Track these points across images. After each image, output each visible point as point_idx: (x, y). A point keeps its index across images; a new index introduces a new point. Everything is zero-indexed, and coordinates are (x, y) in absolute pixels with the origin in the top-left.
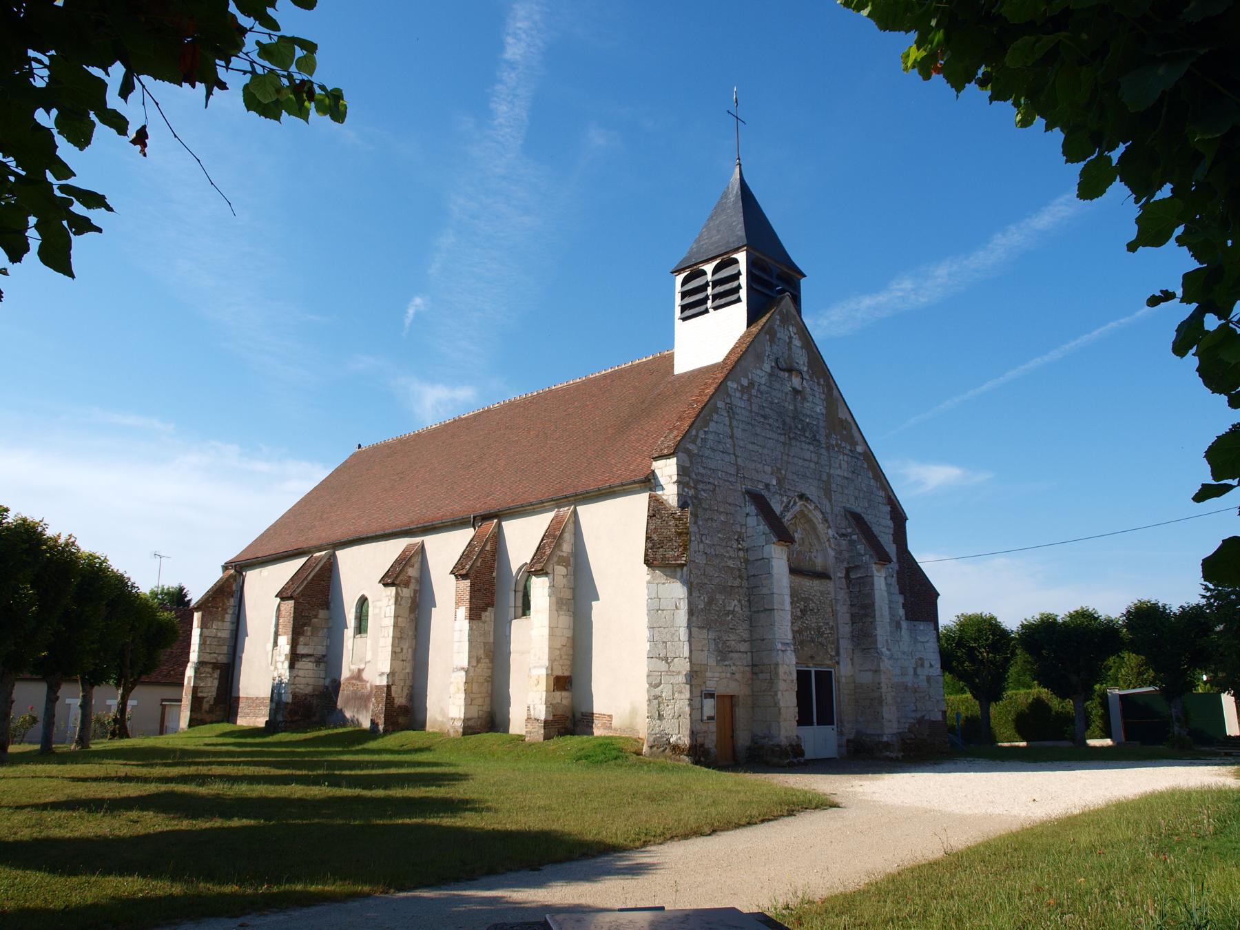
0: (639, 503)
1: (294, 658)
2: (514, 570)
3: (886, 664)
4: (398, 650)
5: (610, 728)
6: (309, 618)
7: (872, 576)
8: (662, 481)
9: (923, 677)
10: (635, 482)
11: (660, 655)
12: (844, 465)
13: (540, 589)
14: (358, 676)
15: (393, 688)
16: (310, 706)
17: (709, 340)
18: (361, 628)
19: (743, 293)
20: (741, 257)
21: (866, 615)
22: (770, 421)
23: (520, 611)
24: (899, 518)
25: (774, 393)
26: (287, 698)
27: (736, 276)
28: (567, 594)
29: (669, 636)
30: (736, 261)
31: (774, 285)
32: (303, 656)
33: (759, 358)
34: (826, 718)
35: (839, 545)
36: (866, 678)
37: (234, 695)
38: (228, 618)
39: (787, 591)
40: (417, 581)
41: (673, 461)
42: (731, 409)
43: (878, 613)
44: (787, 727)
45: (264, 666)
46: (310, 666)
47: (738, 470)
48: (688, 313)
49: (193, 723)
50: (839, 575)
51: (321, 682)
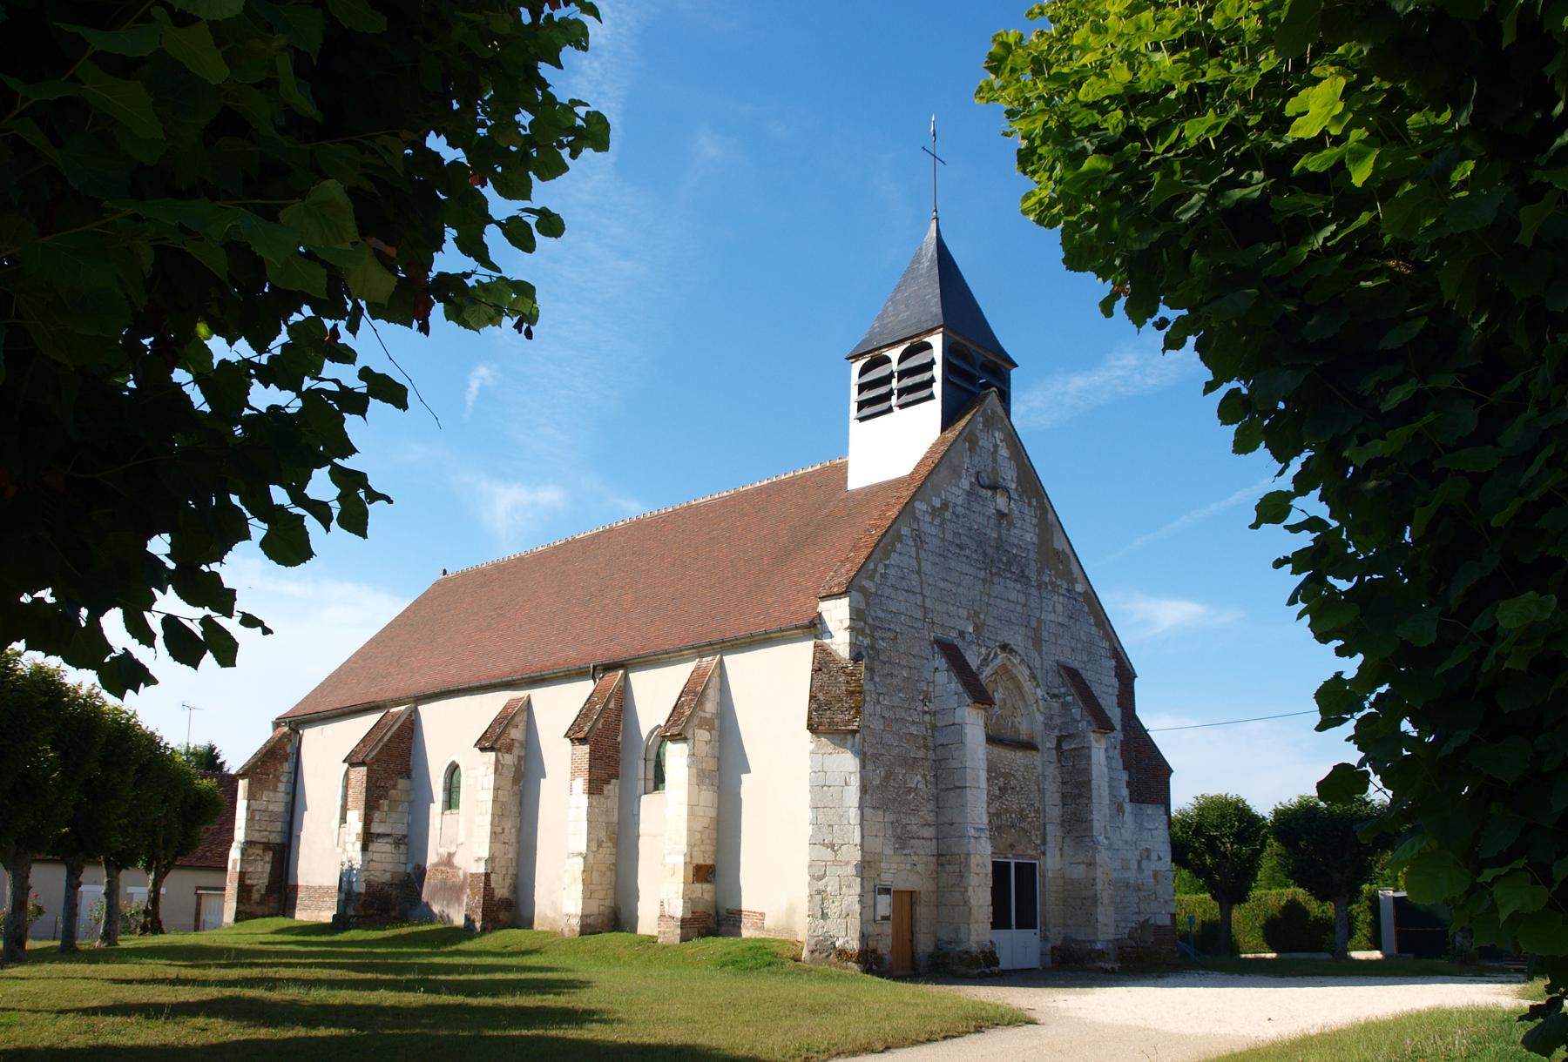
0: (801, 654)
1: (368, 838)
2: (644, 733)
3: (1103, 856)
4: (499, 830)
5: (762, 928)
6: (386, 789)
7: (1089, 748)
8: (831, 626)
9: (1148, 873)
10: (797, 628)
11: (825, 842)
12: (1059, 608)
13: (677, 757)
14: (448, 861)
15: (493, 877)
16: (386, 897)
17: (894, 446)
18: (451, 802)
19: (937, 388)
20: (936, 341)
21: (1080, 795)
22: (968, 552)
23: (651, 784)
24: (1125, 675)
25: (973, 516)
26: (360, 888)
27: (929, 366)
28: (711, 765)
29: (836, 818)
30: (928, 346)
31: (977, 376)
32: (379, 836)
33: (956, 472)
34: (1027, 920)
35: (1049, 708)
36: (1078, 872)
37: (291, 882)
38: (282, 787)
39: (983, 765)
40: (522, 745)
41: (845, 601)
42: (918, 538)
43: (1095, 793)
44: (978, 930)
45: (329, 850)
46: (388, 848)
47: (926, 613)
48: (867, 411)
49: (240, 916)
50: (1049, 745)
51: (402, 868)
